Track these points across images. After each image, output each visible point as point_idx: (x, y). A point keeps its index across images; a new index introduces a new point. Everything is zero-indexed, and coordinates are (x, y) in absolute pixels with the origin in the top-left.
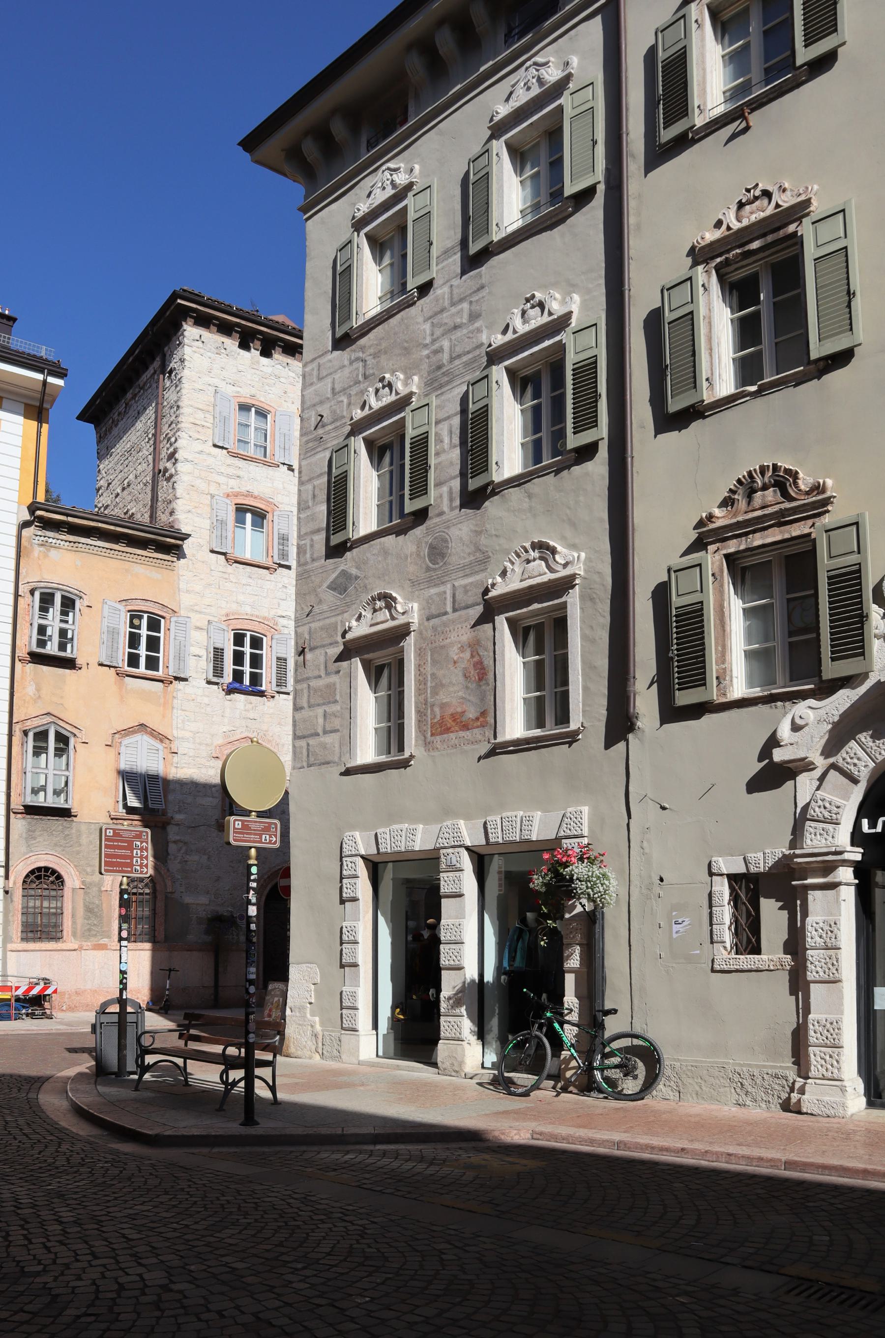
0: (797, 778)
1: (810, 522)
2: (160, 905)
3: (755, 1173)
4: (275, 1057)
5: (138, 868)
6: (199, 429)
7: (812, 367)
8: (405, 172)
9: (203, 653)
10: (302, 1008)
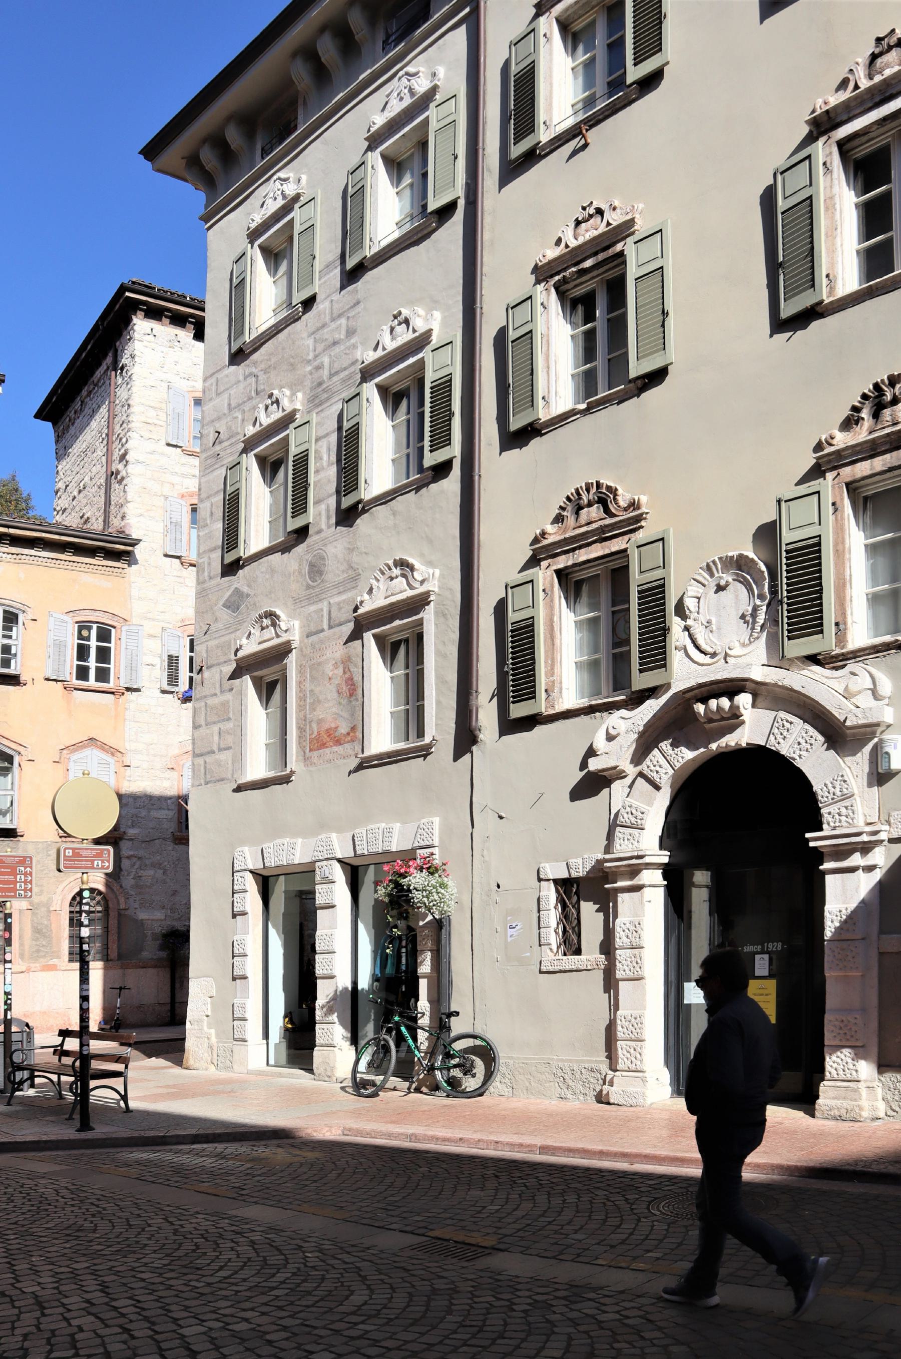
1: (626, 537)
2: (113, 922)
3: (505, 1157)
4: (126, 1067)
5: (22, 892)
6: (151, 428)
7: (632, 385)
8: (294, 182)
9: (157, 661)
10: (200, 1021)
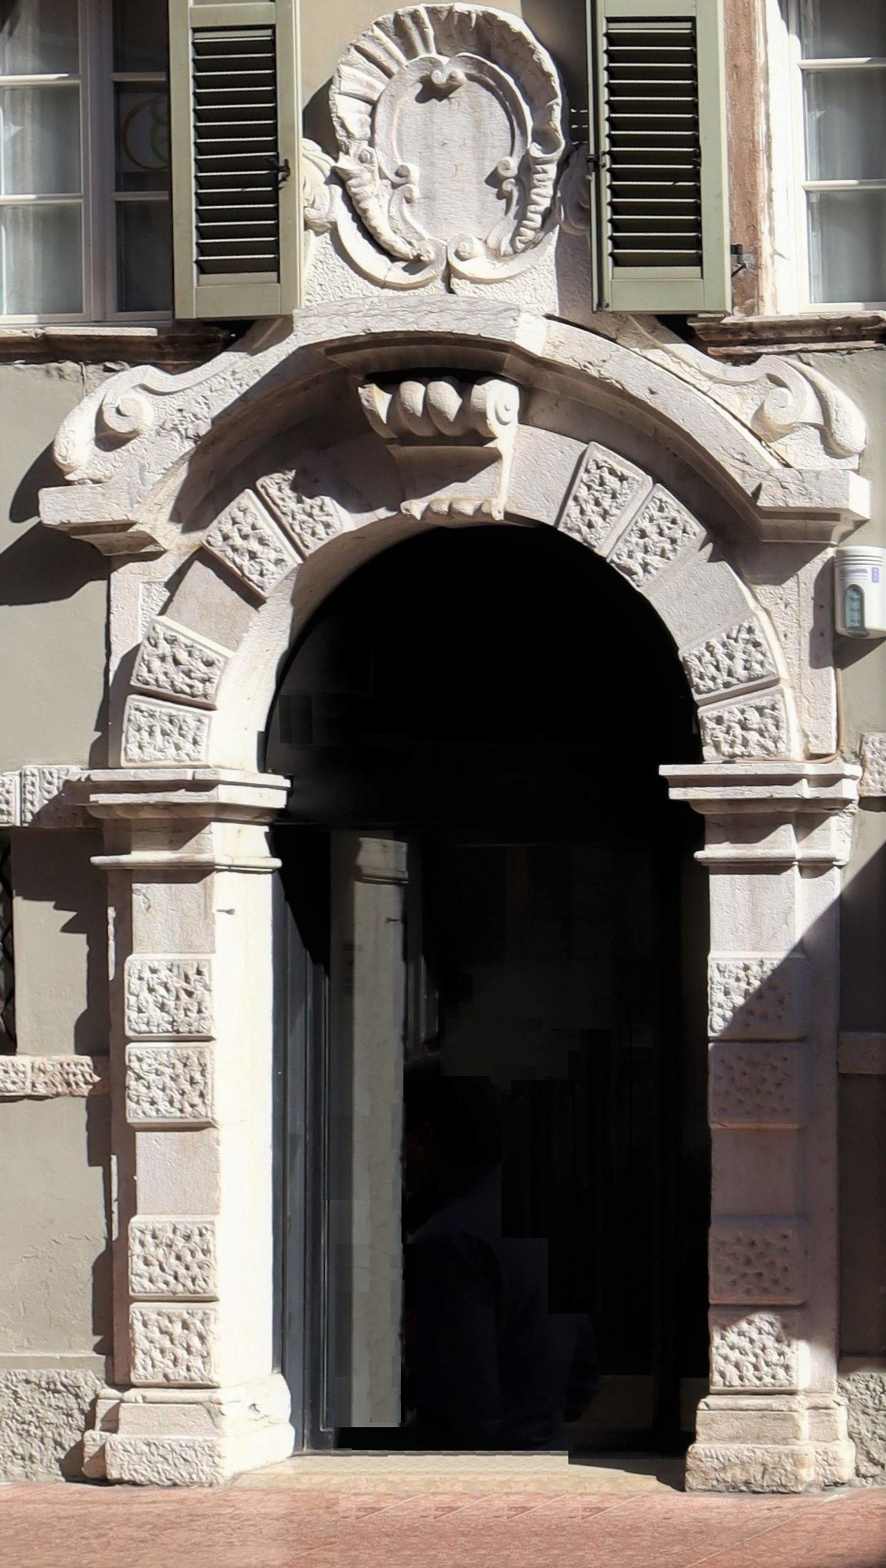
0: (114, 576)
